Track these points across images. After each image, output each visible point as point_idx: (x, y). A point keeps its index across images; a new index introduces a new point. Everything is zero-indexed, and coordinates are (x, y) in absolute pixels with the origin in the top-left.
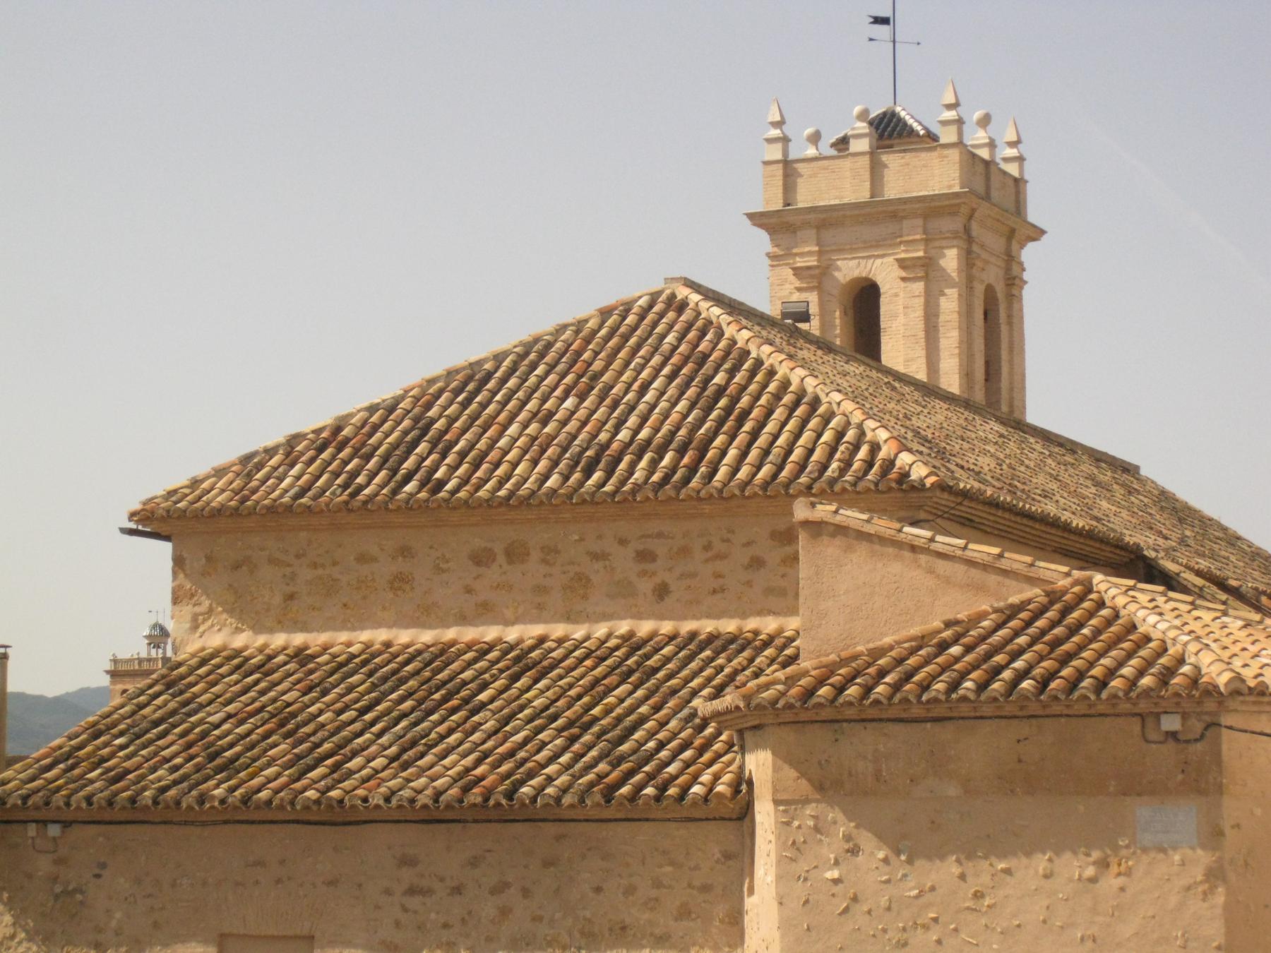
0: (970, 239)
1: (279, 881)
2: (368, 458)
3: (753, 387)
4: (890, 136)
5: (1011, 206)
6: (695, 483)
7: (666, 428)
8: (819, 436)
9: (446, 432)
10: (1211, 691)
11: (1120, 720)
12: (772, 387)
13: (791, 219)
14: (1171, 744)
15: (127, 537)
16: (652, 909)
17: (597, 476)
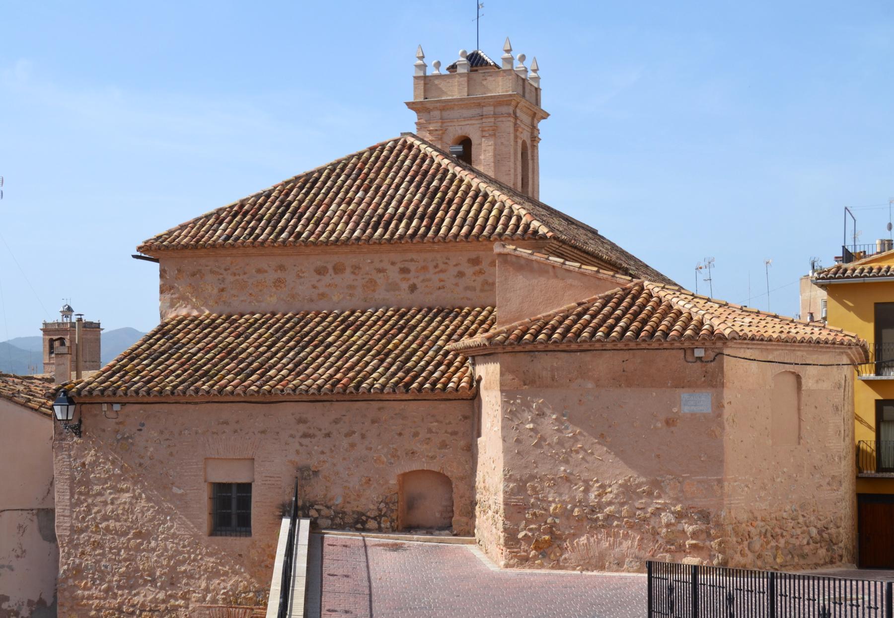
0: (516, 118)
1: (236, 431)
2: (260, 220)
3: (453, 187)
4: (476, 65)
5: (533, 100)
6: (430, 234)
7: (411, 208)
8: (490, 212)
9: (299, 208)
10: (721, 337)
11: (674, 351)
12: (463, 188)
13: (428, 106)
14: (699, 363)
15: (135, 259)
16: (427, 444)
17: (380, 231)
